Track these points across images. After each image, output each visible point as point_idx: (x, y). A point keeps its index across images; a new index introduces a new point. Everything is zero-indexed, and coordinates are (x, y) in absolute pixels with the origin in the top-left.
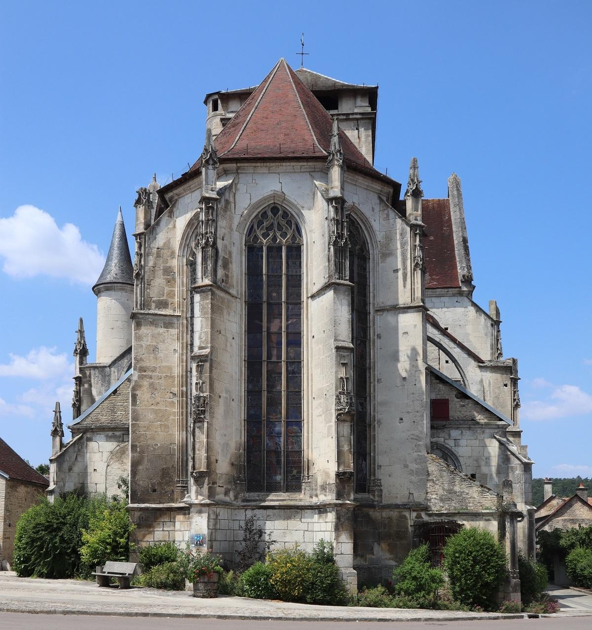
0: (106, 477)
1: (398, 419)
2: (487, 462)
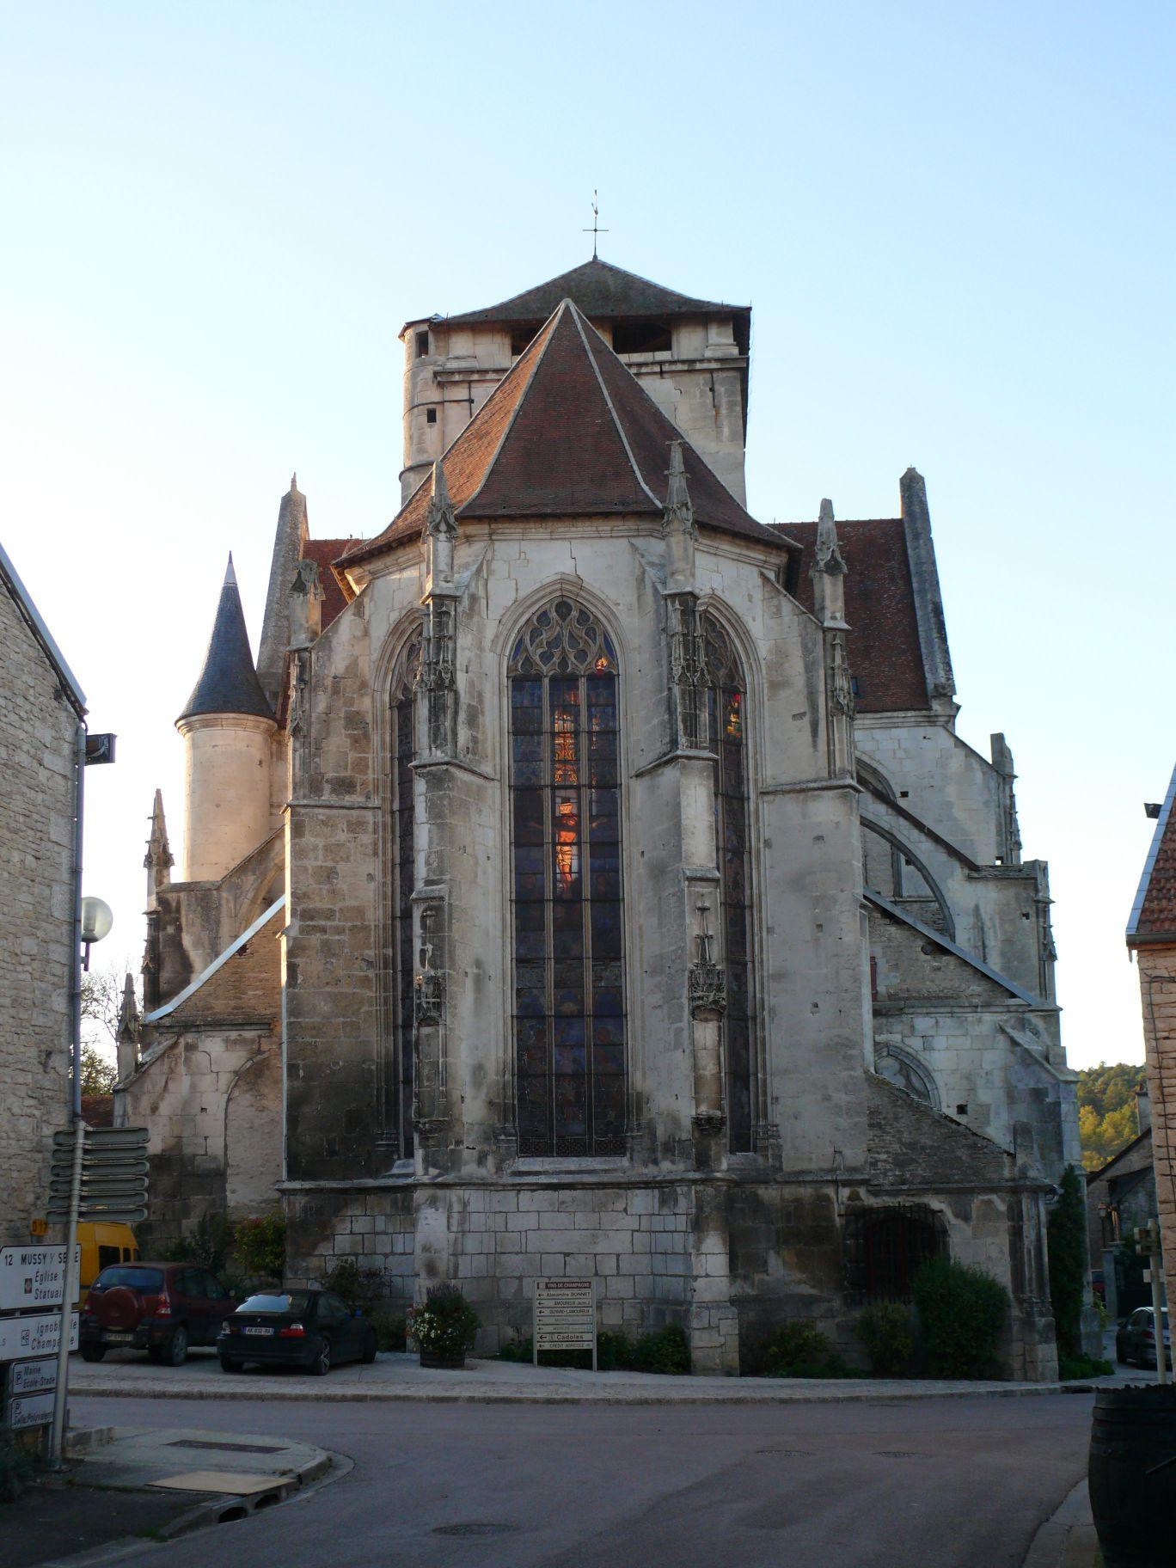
1: (809, 1006)
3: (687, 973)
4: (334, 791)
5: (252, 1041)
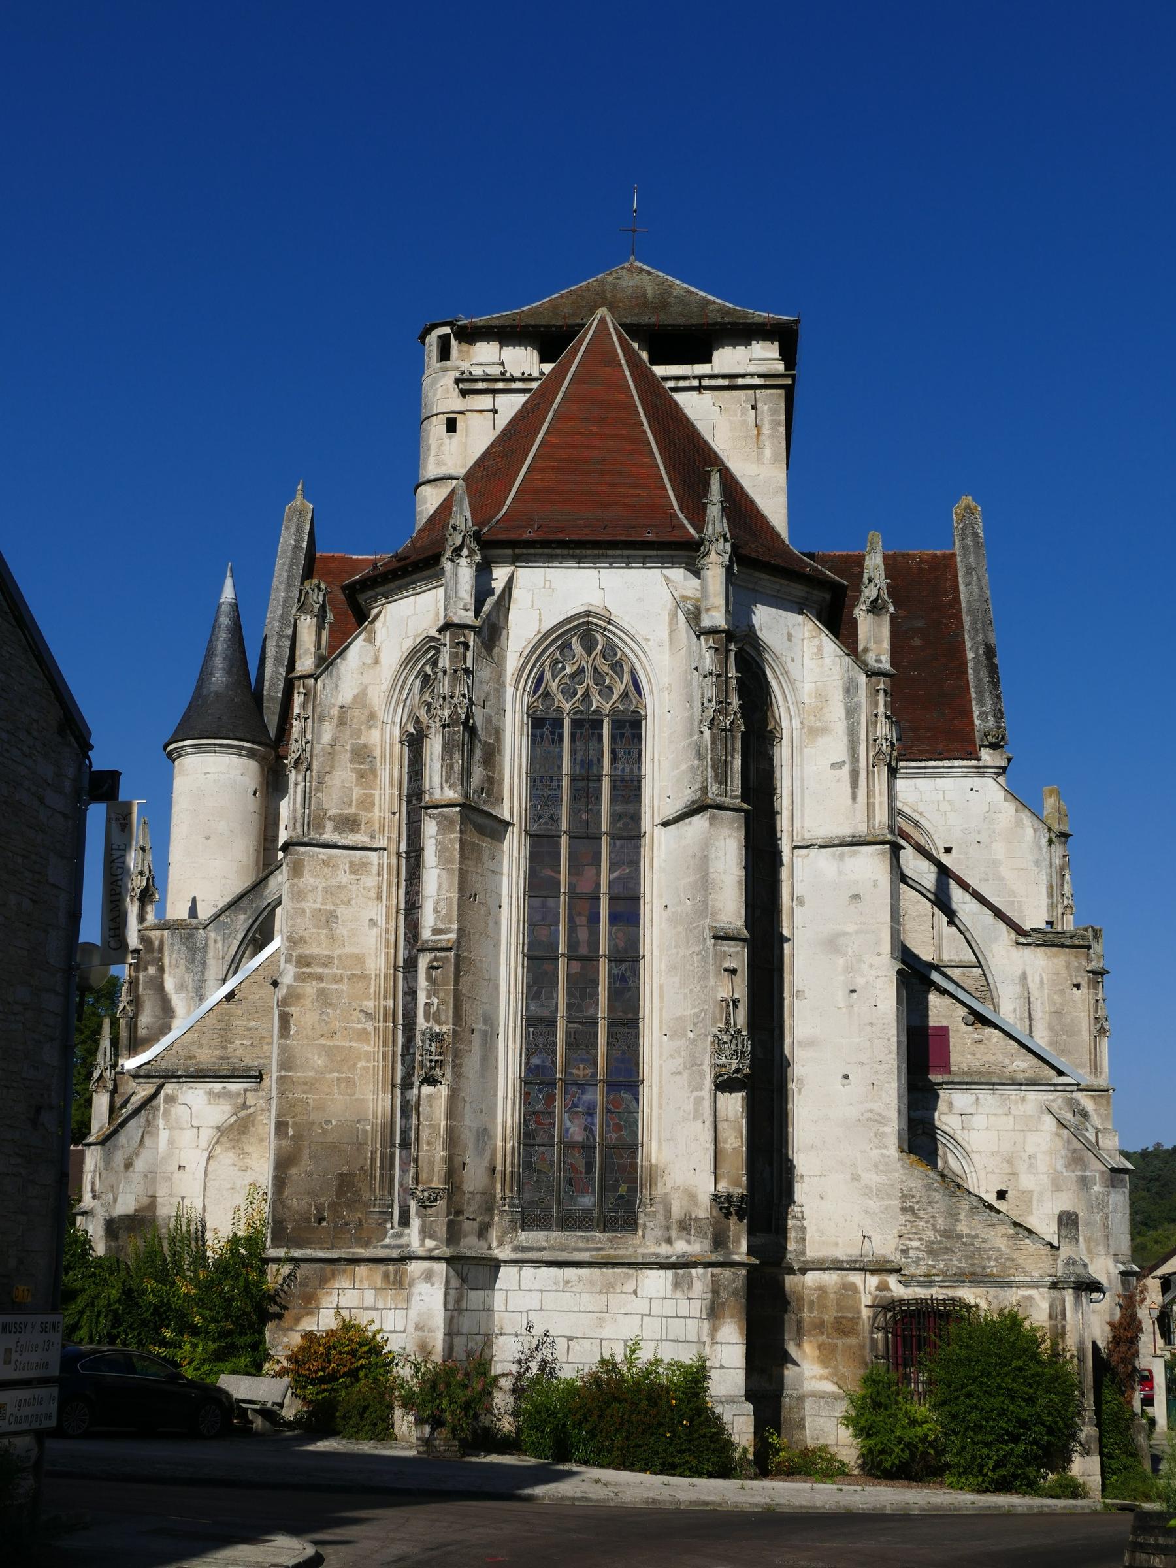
2: (1031, 1165)
3: (710, 1039)
4: (336, 829)
5: (238, 1094)
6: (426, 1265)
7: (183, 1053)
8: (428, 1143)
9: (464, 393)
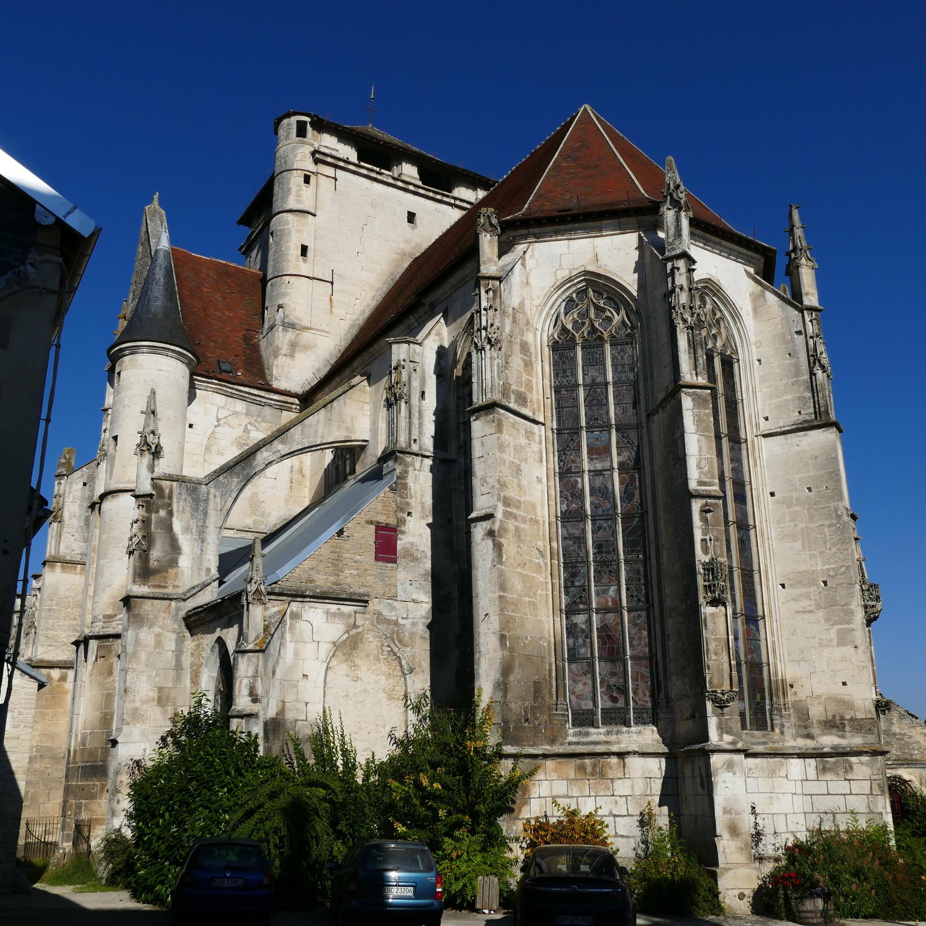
0: (325, 692)
5: (350, 616)
6: (726, 756)
7: (304, 577)
8: (716, 654)
9: (317, 161)
